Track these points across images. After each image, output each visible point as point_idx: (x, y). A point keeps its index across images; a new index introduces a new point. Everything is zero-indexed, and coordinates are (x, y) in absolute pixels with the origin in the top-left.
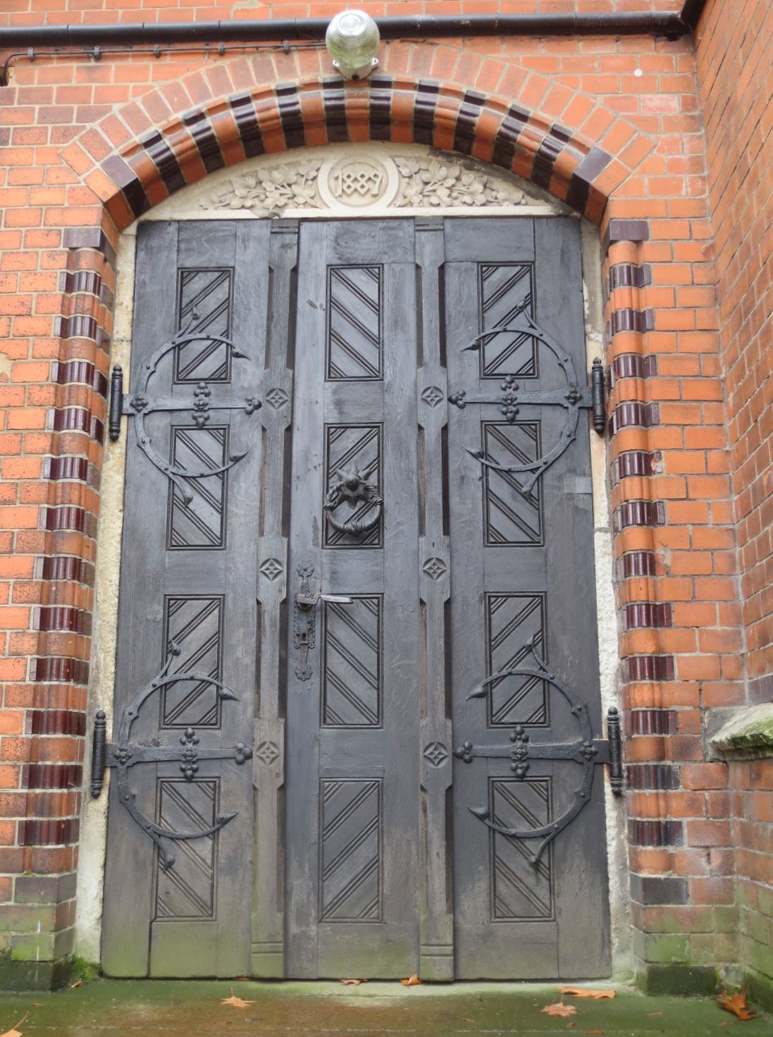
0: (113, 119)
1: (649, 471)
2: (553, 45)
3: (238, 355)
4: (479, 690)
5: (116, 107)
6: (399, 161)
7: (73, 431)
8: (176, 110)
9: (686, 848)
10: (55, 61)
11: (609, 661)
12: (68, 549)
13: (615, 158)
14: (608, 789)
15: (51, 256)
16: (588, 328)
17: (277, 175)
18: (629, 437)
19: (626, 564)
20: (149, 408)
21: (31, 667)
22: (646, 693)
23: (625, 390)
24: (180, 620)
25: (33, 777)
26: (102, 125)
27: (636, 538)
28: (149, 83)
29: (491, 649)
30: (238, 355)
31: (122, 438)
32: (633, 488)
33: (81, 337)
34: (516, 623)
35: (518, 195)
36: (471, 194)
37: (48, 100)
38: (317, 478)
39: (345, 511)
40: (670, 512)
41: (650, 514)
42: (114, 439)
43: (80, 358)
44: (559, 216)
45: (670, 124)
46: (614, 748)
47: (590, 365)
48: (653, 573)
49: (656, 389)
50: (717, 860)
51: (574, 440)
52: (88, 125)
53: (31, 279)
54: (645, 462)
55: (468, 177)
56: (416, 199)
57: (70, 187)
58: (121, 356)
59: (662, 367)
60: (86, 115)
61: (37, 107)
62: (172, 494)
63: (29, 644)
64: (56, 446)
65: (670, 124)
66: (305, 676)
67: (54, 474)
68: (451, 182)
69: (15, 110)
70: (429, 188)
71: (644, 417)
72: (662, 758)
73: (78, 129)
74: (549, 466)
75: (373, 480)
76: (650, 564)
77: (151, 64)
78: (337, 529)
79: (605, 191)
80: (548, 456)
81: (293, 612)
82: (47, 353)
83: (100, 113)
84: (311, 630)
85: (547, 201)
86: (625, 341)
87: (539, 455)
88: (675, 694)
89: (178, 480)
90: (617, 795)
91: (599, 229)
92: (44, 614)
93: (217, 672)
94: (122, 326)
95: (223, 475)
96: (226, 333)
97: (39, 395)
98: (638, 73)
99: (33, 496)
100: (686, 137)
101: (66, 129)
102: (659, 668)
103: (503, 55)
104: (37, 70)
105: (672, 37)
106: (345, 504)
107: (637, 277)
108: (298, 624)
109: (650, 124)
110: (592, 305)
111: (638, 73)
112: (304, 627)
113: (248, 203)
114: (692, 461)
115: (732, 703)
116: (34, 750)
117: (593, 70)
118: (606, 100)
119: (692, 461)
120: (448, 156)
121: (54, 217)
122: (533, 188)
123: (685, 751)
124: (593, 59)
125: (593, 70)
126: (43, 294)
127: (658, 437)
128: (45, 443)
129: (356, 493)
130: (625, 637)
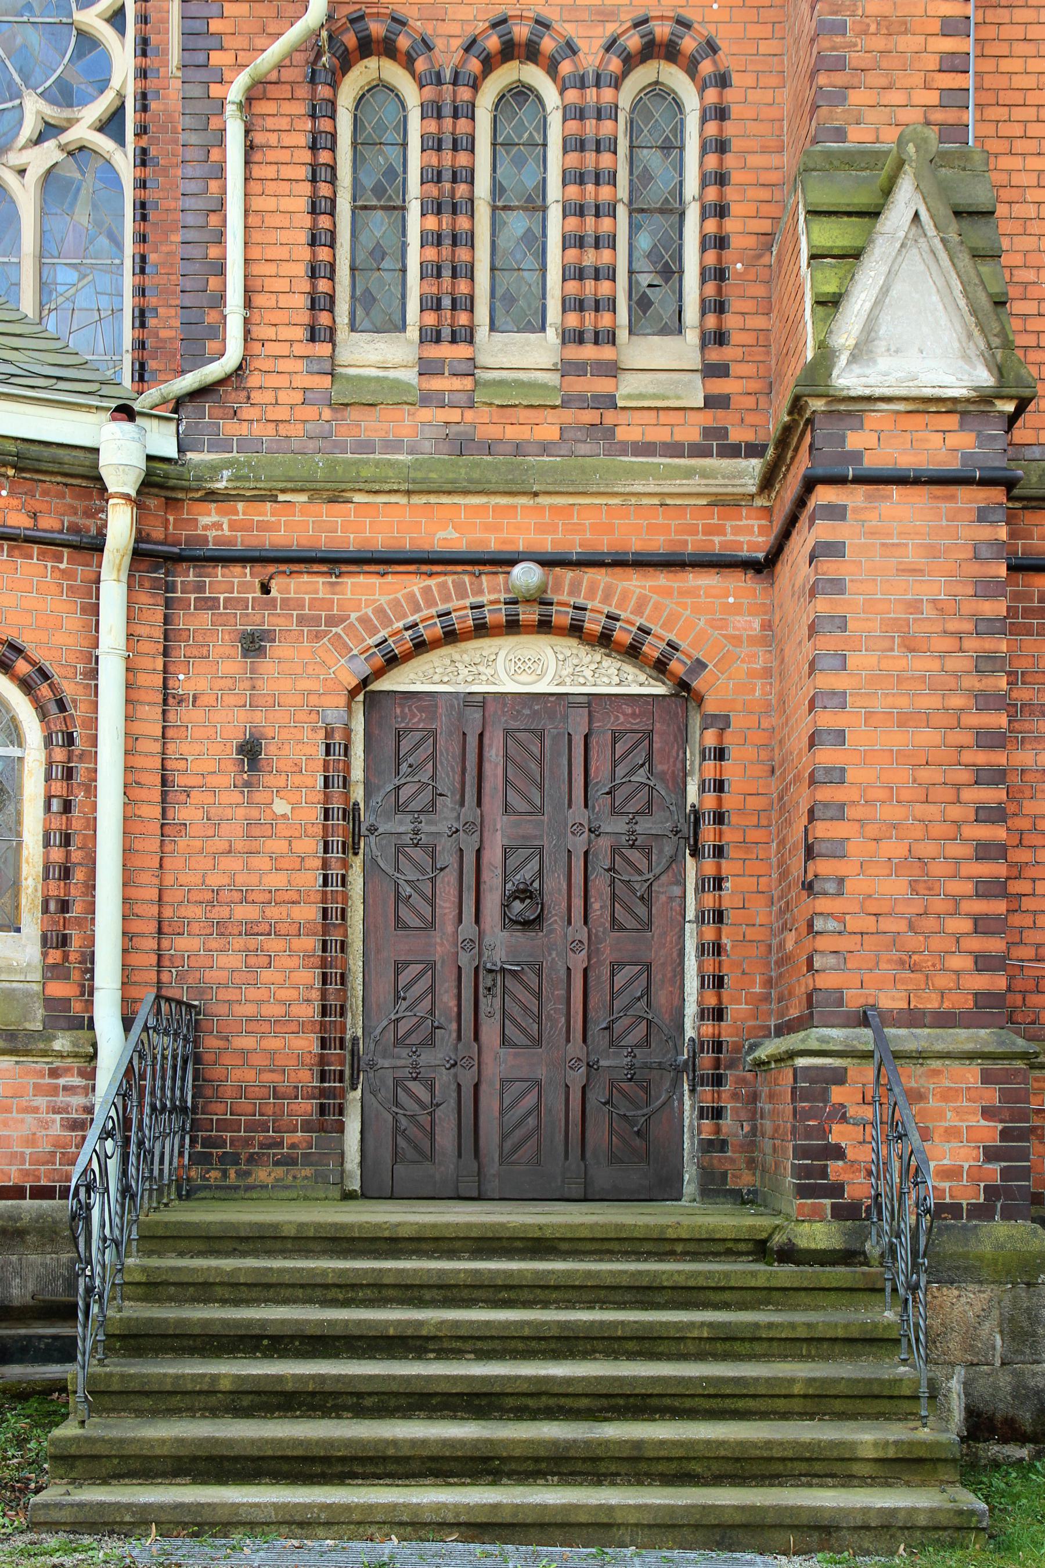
0: (352, 624)
1: (720, 889)
2: (671, 576)
3: (441, 795)
4: (604, 1025)
5: (354, 616)
6: (557, 649)
7: (335, 855)
8: (398, 620)
9: (729, 1121)
10: (863, 1453)
11: (691, 1009)
12: (336, 937)
13: (710, 666)
14: (686, 1087)
15: (314, 729)
16: (689, 779)
17: (466, 658)
18: (709, 866)
19: (702, 950)
20: (380, 831)
21: (318, 1010)
22: (708, 1029)
23: (708, 834)
24: (404, 978)
25: (323, 1077)
26: (343, 629)
27: (709, 933)
28: (377, 597)
29: (612, 999)
30: (441, 795)
31: (361, 851)
32: (709, 900)
33: (336, 790)
34: (631, 981)
35: (642, 677)
36: (608, 676)
37: (303, 608)
38: (498, 881)
39: (517, 906)
40: (730, 917)
41: (719, 916)
42: (356, 854)
43: (336, 805)
44: (672, 695)
45: (752, 640)
46: (692, 1064)
47: (688, 808)
48: (719, 954)
49: (730, 835)
50: (747, 1128)
51: (676, 859)
52: (334, 630)
53: (300, 746)
54: (718, 882)
55: (607, 662)
56: (568, 680)
57: (510, 922)
58: (358, 794)
59: (734, 819)
60: (332, 621)
61: (295, 613)
62: (397, 894)
63: (315, 995)
64: (325, 865)
65: (752, 640)
66: (490, 1015)
67: (325, 884)
68: (593, 666)
69: (279, 615)
70: (578, 669)
71: (719, 852)
72: (718, 1068)
73: (327, 633)
74: (657, 878)
75: (536, 885)
76: (718, 949)
77: (376, 580)
78: (511, 920)
79: (703, 691)
80: (657, 871)
81: (482, 973)
82: (316, 800)
83: (343, 619)
84: (494, 985)
85: (664, 683)
86: (710, 801)
87: (650, 870)
88: (727, 1032)
89: (401, 882)
90: (693, 1091)
91: (700, 706)
92: (324, 975)
93: (432, 1012)
94: (357, 773)
95: (433, 880)
96: (433, 777)
97: (311, 830)
98: (731, 600)
99: (312, 899)
100: (760, 651)
101: (318, 632)
102: (718, 1014)
103: (634, 583)
104: (293, 583)
105: (759, 571)
106: (517, 902)
107: (720, 754)
108: (485, 981)
109: (736, 640)
110: (692, 763)
111: (731, 600)
112: (489, 984)
113: (445, 679)
114: (750, 883)
115: (765, 1036)
116: (322, 1060)
117: (699, 596)
118: (707, 621)
119: (750, 883)
120: (593, 646)
121: (314, 700)
122: (654, 674)
123: (732, 1065)
124: (699, 587)
125: (699, 596)
126: (310, 758)
127: (727, 867)
128: (318, 863)
129: (524, 893)
130: (700, 994)
